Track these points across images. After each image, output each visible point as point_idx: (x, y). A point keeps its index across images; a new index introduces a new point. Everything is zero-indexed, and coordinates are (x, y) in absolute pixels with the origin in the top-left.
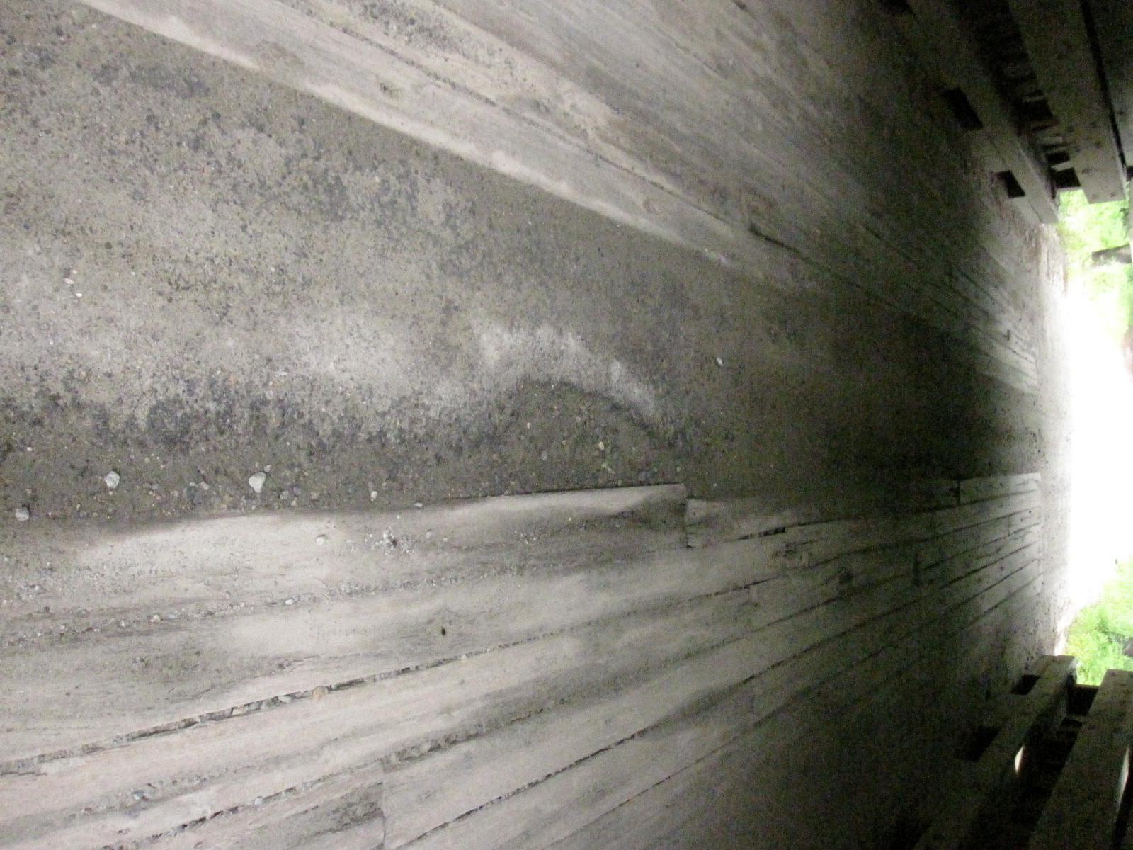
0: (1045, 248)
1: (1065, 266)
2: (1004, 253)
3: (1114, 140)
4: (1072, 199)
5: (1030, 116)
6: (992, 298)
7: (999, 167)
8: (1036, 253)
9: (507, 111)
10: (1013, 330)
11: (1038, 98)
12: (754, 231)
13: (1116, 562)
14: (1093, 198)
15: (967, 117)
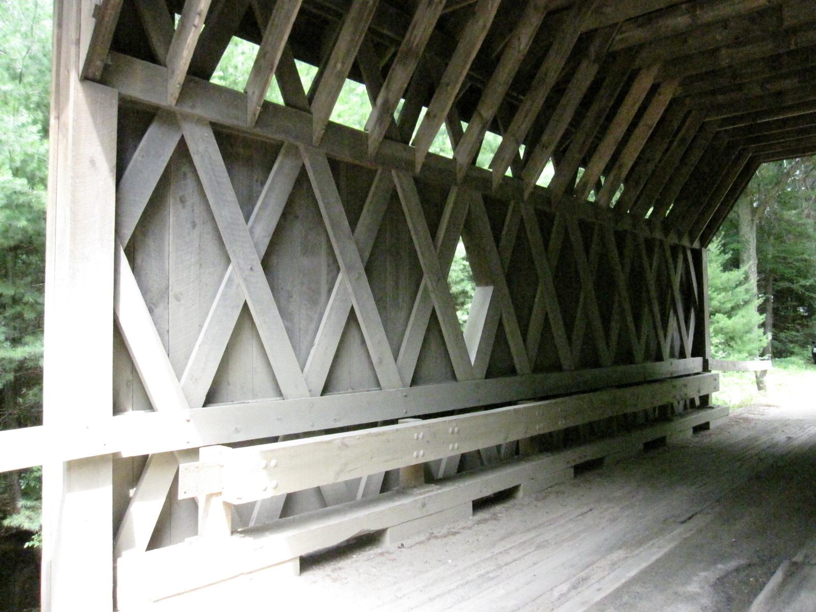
0: (746, 415)
1: (762, 406)
2: (741, 434)
3: (686, 378)
4: (716, 399)
5: (666, 414)
6: (768, 447)
7: (691, 432)
8: (746, 420)
9: (613, 571)
10: (787, 435)
11: (657, 409)
12: (683, 522)
13: (188, 421)
14: (716, 389)
15: (659, 443)
